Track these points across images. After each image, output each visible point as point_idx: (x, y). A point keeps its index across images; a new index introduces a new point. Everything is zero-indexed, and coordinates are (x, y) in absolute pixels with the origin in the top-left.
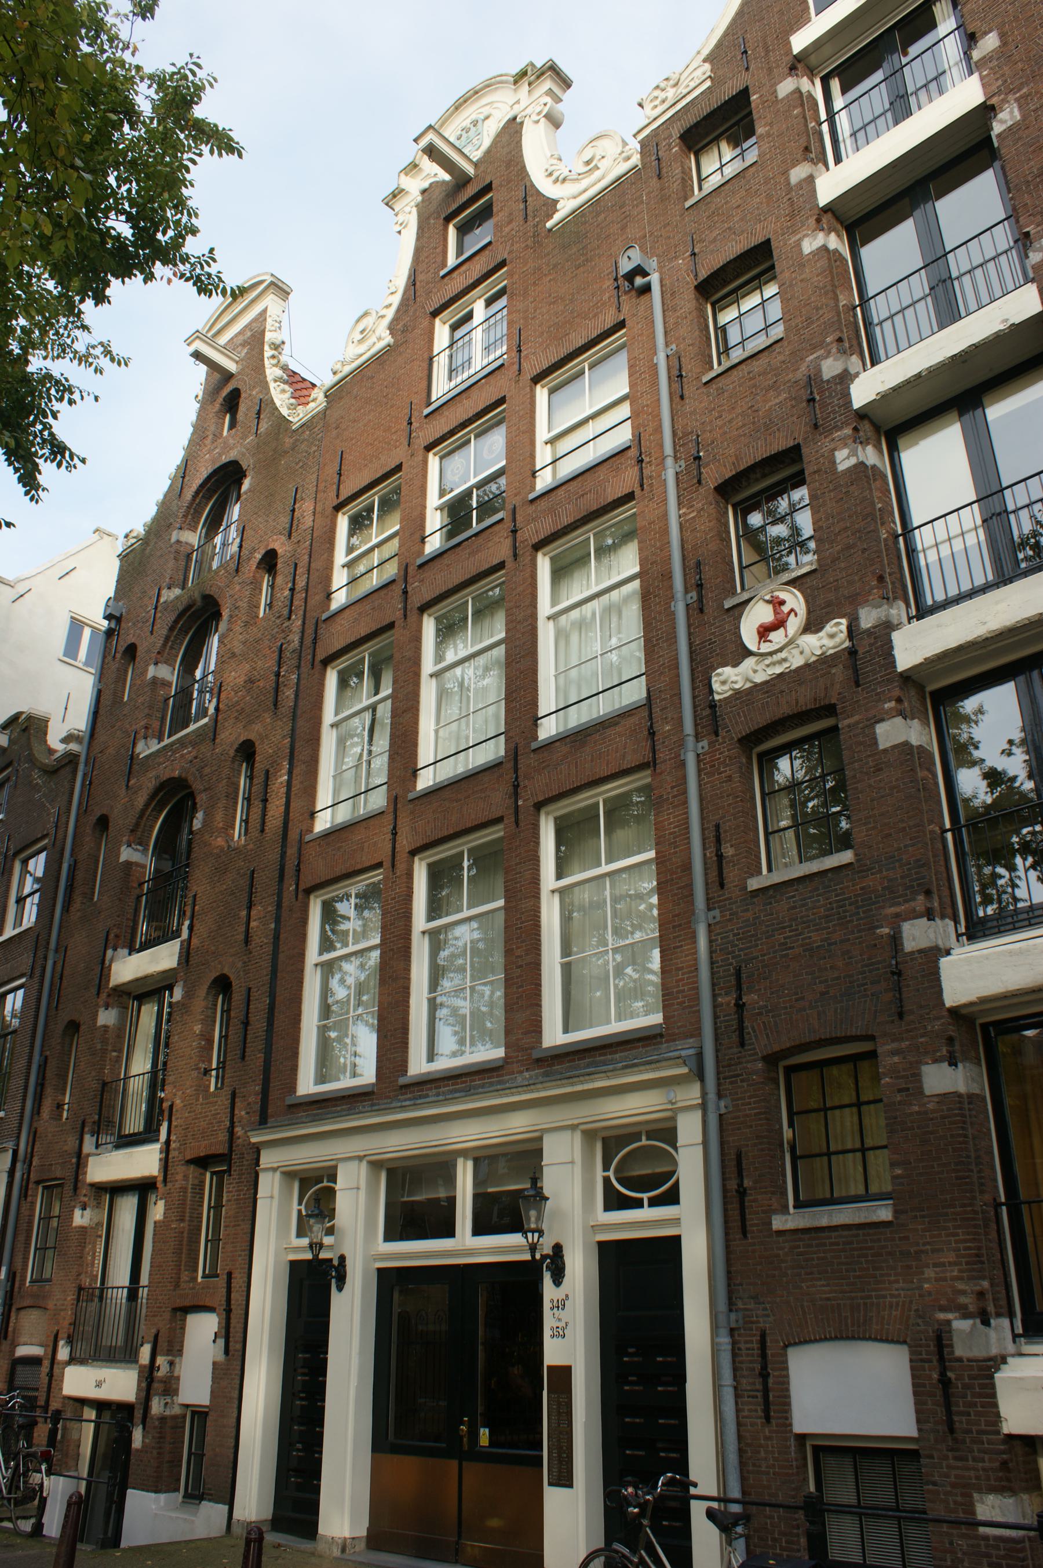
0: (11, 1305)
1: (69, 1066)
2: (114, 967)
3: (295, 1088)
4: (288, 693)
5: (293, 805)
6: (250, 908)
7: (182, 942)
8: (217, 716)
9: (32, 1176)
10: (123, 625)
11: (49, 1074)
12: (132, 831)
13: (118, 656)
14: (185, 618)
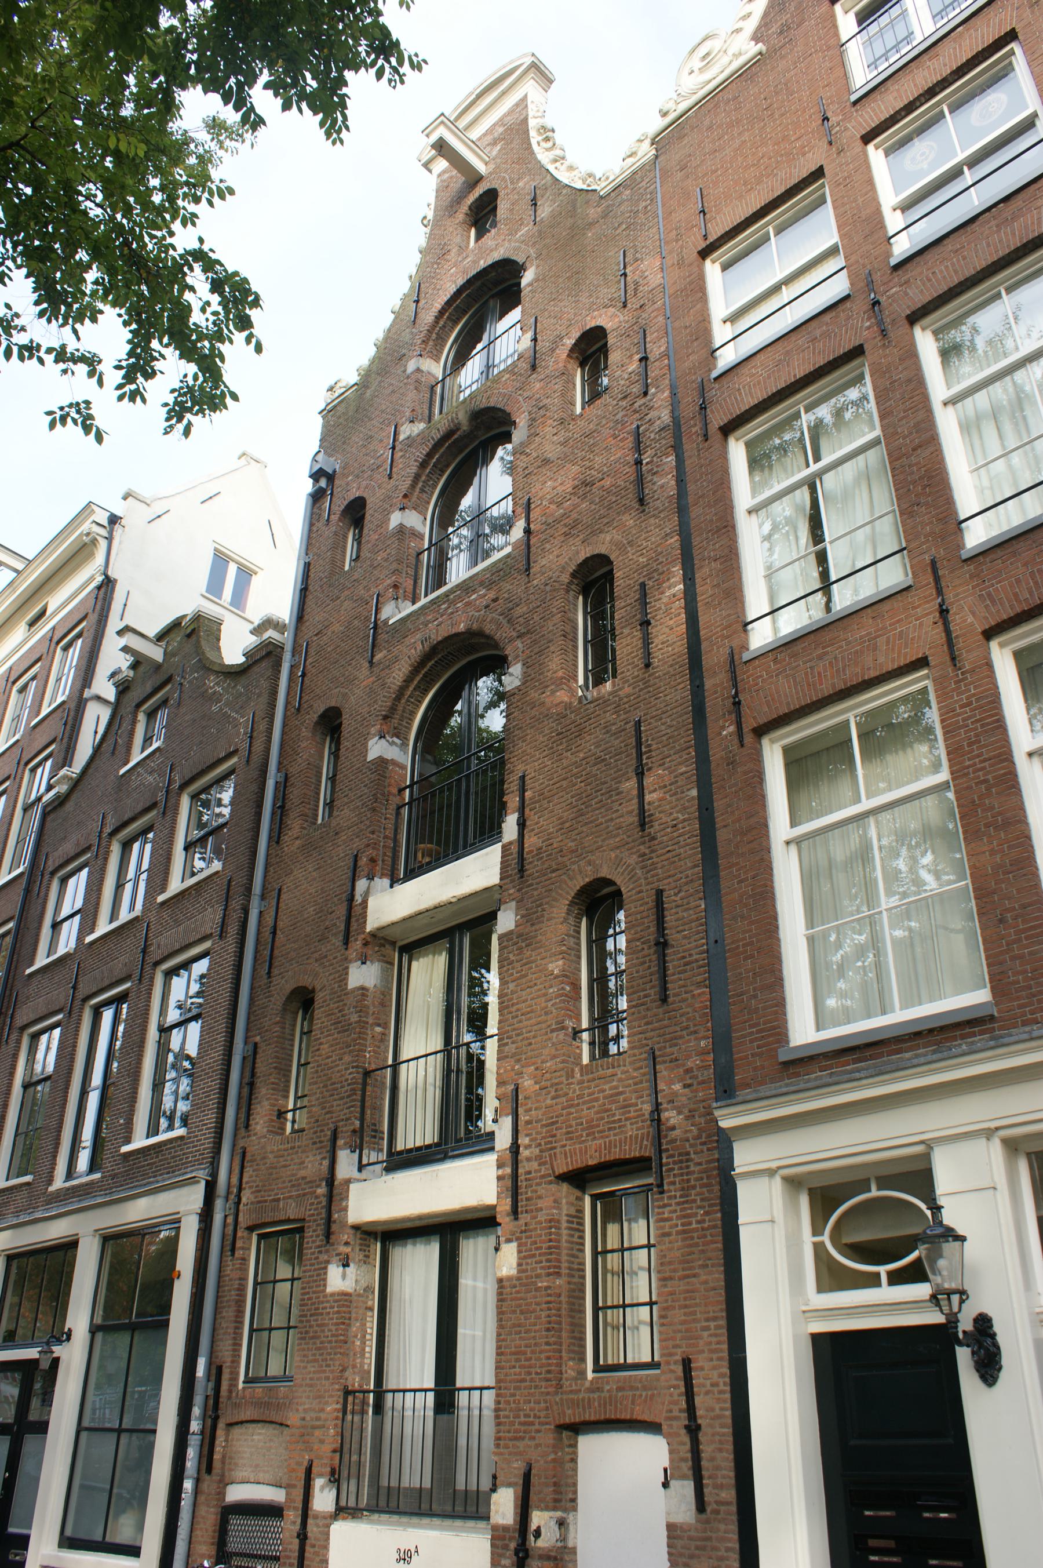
0: (216, 1419)
1: (292, 1056)
2: (371, 902)
3: (786, 1035)
4: (664, 483)
5: (703, 619)
6: (640, 774)
7: (505, 848)
8: (529, 540)
9: (241, 1218)
10: (337, 482)
11: (261, 1067)
12: (385, 718)
13: (334, 518)
14: (442, 450)
